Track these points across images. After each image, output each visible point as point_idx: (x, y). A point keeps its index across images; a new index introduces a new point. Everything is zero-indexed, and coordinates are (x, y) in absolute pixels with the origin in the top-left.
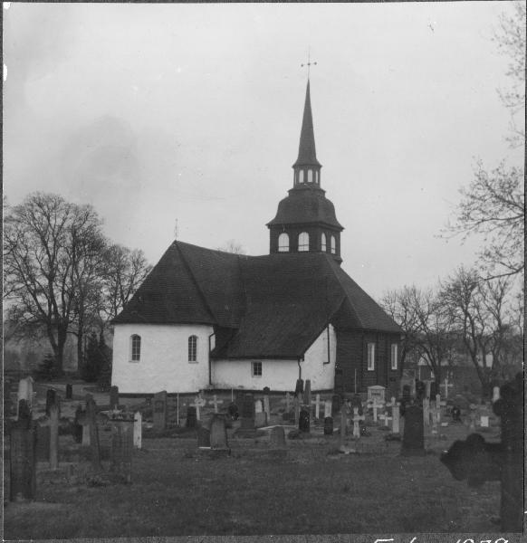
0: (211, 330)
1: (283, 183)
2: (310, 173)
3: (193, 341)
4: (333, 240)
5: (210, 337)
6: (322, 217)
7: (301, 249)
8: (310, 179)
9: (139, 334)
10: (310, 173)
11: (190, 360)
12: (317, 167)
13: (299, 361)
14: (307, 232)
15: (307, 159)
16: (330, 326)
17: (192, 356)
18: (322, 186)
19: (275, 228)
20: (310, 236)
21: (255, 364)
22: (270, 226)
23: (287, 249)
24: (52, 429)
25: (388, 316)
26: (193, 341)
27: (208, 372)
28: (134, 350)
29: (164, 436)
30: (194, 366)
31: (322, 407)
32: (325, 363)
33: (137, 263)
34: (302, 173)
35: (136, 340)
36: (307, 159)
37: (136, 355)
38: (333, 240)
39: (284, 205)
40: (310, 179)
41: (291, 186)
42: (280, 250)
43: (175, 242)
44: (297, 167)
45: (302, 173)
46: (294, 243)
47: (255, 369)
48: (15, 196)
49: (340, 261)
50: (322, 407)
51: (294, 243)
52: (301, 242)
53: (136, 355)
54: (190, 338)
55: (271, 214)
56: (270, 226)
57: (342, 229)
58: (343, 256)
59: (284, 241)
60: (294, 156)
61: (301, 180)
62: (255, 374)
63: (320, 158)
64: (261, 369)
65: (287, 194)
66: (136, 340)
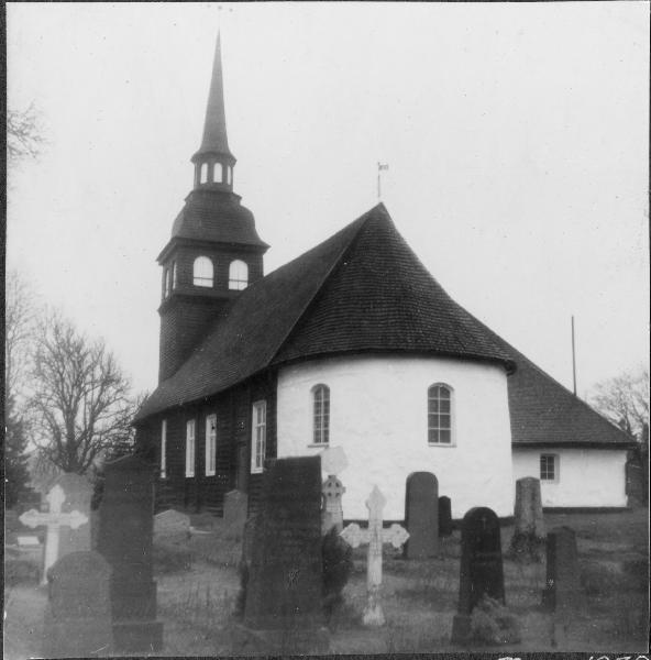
1: (176, 187)
2: (218, 168)
7: (232, 286)
8: (218, 178)
10: (218, 168)
12: (227, 160)
14: (243, 259)
15: (215, 151)
16: (210, 422)
18: (236, 190)
23: (209, 284)
25: (138, 429)
31: (609, 555)
34: (205, 168)
35: (321, 393)
36: (215, 151)
40: (218, 178)
42: (197, 283)
44: (199, 159)
45: (205, 168)
46: (221, 276)
50: (609, 555)
51: (221, 276)
52: (197, 273)
60: (195, 144)
61: (204, 180)
63: (234, 147)
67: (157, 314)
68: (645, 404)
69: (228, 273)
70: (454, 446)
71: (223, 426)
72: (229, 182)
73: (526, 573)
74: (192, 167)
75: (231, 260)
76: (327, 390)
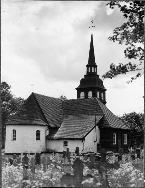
0: (47, 128)
1: (82, 72)
2: (93, 68)
3: (38, 133)
4: (102, 94)
5: (46, 131)
6: (98, 86)
9: (16, 130)
10: (93, 68)
11: (37, 140)
12: (96, 66)
13: (82, 141)
14: (91, 91)
15: (92, 63)
17: (38, 138)
18: (98, 74)
19: (79, 90)
20: (85, 93)
21: (65, 142)
22: (77, 89)
24: (79, 149)
26: (38, 133)
27: (45, 144)
28: (13, 136)
29: (122, 145)
30: (38, 142)
32: (94, 141)
33: (141, 115)
34: (89, 69)
35: (14, 131)
37: (14, 138)
38: (102, 94)
39: (82, 81)
40: (93, 71)
41: (86, 74)
43: (33, 93)
44: (88, 66)
45: (89, 69)
46: (86, 96)
47: (65, 144)
48: (2, 81)
49: (104, 103)
51: (86, 96)
53: (14, 138)
54: (37, 131)
55: (78, 84)
56: (77, 89)
57: (106, 90)
58: (107, 100)
59: (82, 94)
60: (86, 62)
61: (89, 71)
62: (65, 146)
64: (67, 144)
65: (84, 77)
66: (14, 131)
67: (132, 112)
68: (43, 13)
69: (80, 95)
70: (40, 141)
71: (30, 157)
72: (96, 72)
73: (111, 162)
74: (86, 68)
75: (89, 91)
76: (16, 131)
